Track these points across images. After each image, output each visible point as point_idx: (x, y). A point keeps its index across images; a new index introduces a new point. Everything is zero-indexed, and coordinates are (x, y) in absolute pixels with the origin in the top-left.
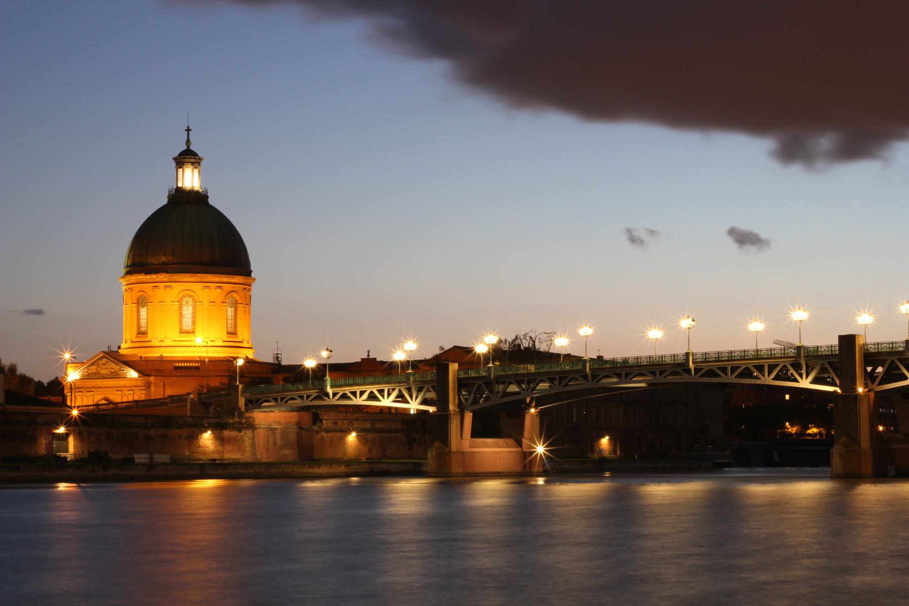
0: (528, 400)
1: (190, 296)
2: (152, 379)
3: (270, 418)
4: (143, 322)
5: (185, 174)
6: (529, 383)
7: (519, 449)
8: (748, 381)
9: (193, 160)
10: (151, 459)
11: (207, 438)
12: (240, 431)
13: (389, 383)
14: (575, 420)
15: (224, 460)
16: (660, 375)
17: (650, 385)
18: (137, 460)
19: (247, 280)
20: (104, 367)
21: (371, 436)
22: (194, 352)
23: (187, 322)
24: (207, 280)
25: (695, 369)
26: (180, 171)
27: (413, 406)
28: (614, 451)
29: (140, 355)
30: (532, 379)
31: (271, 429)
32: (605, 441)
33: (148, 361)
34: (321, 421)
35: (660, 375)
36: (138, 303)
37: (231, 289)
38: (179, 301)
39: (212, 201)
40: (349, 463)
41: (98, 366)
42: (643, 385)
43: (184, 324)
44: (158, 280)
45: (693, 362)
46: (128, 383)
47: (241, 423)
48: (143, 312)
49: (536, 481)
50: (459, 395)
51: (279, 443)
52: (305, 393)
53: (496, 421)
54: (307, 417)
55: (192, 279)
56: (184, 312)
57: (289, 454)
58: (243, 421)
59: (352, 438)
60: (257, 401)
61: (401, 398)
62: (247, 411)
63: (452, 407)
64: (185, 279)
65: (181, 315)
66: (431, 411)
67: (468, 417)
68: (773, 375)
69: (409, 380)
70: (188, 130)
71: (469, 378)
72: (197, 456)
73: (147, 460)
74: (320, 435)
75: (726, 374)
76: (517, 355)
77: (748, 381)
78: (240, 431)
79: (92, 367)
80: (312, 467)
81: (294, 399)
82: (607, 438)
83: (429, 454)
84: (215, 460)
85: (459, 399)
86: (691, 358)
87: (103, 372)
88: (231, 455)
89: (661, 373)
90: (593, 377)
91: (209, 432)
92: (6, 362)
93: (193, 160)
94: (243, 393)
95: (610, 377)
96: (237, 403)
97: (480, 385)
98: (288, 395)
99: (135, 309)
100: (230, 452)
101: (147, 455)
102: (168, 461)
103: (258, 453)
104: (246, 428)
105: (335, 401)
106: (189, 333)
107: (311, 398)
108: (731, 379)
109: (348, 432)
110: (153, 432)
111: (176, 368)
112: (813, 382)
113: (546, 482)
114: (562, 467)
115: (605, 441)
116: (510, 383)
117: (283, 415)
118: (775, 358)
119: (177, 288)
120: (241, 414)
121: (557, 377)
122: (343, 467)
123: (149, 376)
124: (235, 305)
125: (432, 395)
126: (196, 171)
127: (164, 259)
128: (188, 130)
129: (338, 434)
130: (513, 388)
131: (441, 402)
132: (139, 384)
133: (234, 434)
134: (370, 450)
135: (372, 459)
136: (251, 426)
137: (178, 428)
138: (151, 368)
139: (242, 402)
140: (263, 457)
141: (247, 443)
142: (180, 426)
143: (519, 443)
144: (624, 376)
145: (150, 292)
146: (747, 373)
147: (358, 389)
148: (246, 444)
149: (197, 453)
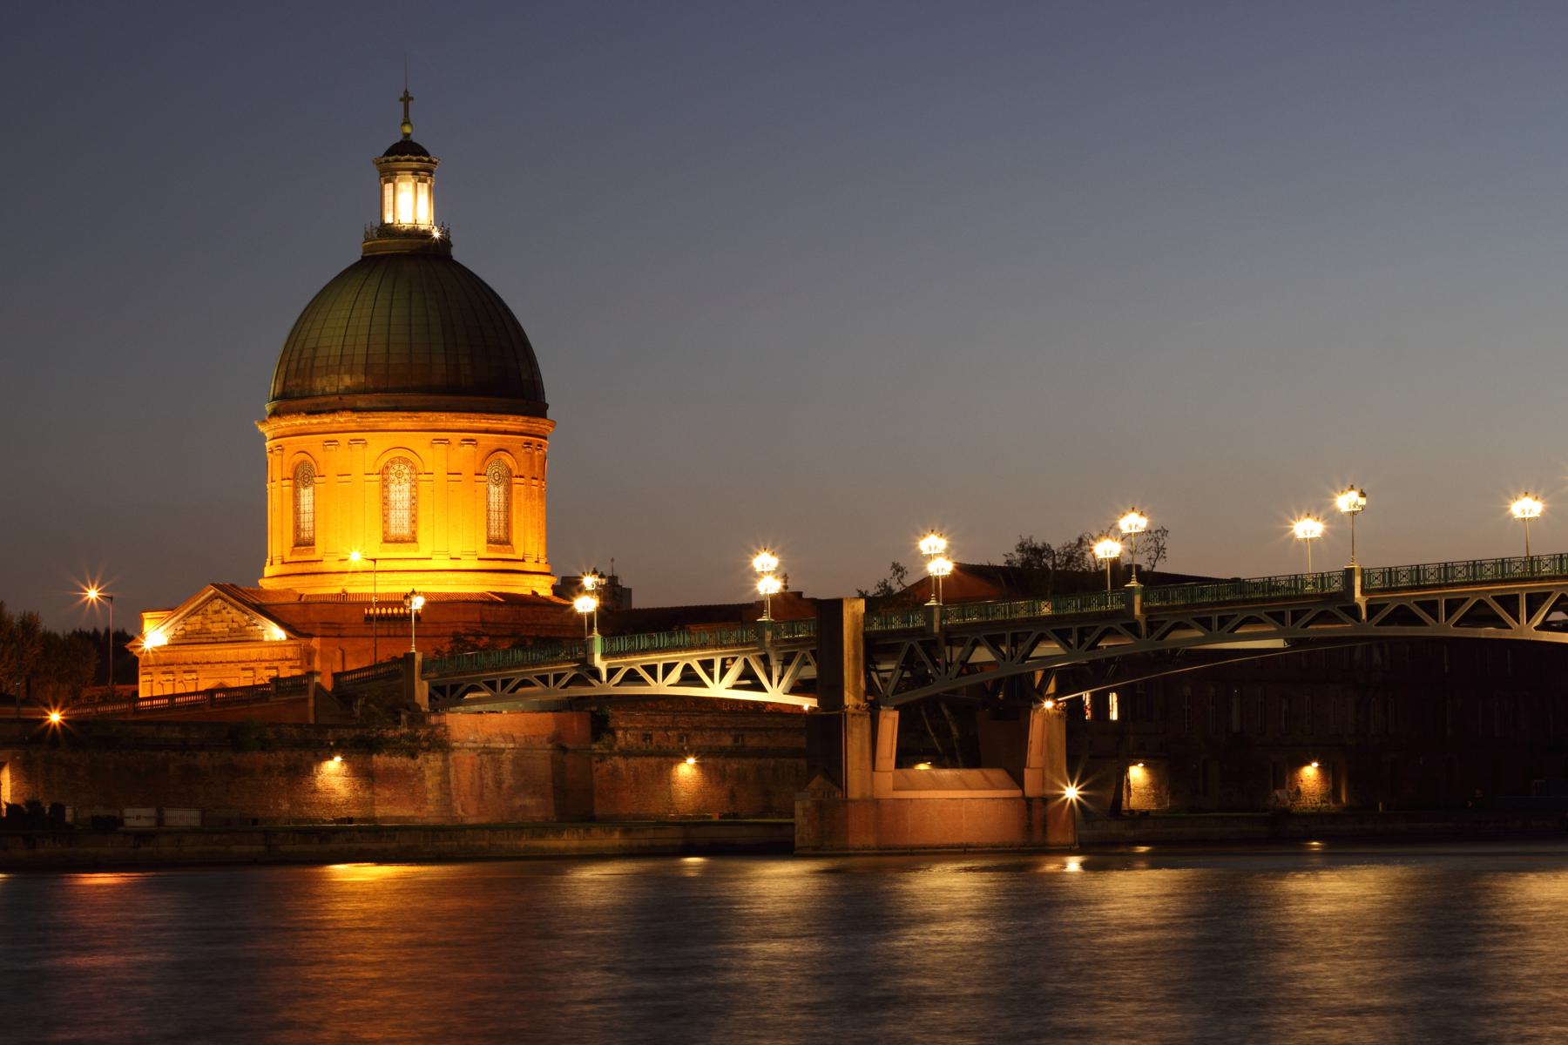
0: (1039, 675)
1: (406, 461)
2: (315, 643)
3: (485, 726)
4: (306, 519)
5: (400, 197)
6: (1015, 642)
7: (1017, 793)
8: (1489, 632)
9: (415, 165)
10: (160, 821)
11: (333, 772)
12: (413, 756)
13: (722, 646)
14: (1236, 728)
15: (374, 819)
16: (1294, 620)
17: (1295, 643)
18: (130, 822)
19: (537, 425)
20: (217, 618)
21: (734, 765)
22: (398, 583)
23: (400, 521)
24: (441, 425)
25: (1369, 608)
26: (388, 188)
27: (775, 694)
28: (1334, 794)
29: (299, 591)
30: (1027, 633)
31: (488, 751)
32: (1310, 773)
33: (305, 603)
34: (612, 732)
35: (1294, 620)
36: (295, 477)
37: (496, 445)
38: (381, 473)
39: (457, 254)
40: (684, 824)
41: (205, 616)
42: (1279, 643)
43: (393, 522)
44: (336, 426)
45: (1363, 592)
46: (266, 653)
47: (414, 739)
48: (306, 496)
49: (1064, 866)
50: (867, 672)
51: (508, 781)
52: (549, 670)
53: (964, 724)
54: (577, 724)
55: (409, 424)
56: (393, 496)
57: (533, 805)
58: (422, 733)
59: (687, 770)
60: (454, 688)
61: (749, 680)
62: (435, 710)
63: (849, 699)
64: (393, 425)
65: (385, 502)
66: (806, 708)
67: (890, 722)
68: (1538, 620)
69: (762, 638)
70: (407, 99)
71: (892, 633)
72: (311, 813)
73: (152, 823)
74: (609, 764)
75: (1436, 618)
76: (1034, 585)
77: (1489, 632)
78: (413, 756)
79: (193, 619)
80: (541, 837)
81: (531, 684)
82: (1315, 765)
83: (798, 805)
84: (350, 820)
85: (869, 681)
86: (1358, 581)
87: (216, 628)
88: (391, 808)
89: (1296, 616)
90: (1152, 627)
91: (338, 759)
92: (15, 611)
93: (415, 165)
94: (423, 671)
95: (1187, 627)
96: (412, 693)
97: (912, 649)
98: (517, 674)
99: (288, 490)
100: (389, 802)
101: (151, 812)
102: (197, 823)
103: (457, 805)
104: (428, 750)
105: (613, 688)
106: (403, 541)
107: (564, 681)
108: (1446, 627)
109: (681, 756)
110: (202, 759)
111: (369, 618)
112: (794, 690)
113: (1084, 865)
114: (1110, 837)
115: (1310, 773)
116: (976, 644)
117: (519, 719)
118: (1542, 579)
119: (377, 444)
120: (417, 718)
121: (1075, 628)
122: (617, 835)
123: (311, 636)
124: (507, 479)
125: (810, 672)
126: (424, 189)
127: (347, 381)
128: (407, 99)
129: (653, 761)
130: (982, 655)
131: (825, 685)
132: (289, 655)
133: (398, 761)
134: (732, 796)
135: (735, 816)
136: (441, 744)
137: (263, 749)
138: (310, 619)
139: (422, 691)
140: (467, 811)
141: (431, 782)
142: (265, 746)
143: (1019, 781)
144: (1215, 624)
145: (319, 455)
146: (1480, 615)
147: (660, 660)
148: (429, 784)
149: (310, 805)
